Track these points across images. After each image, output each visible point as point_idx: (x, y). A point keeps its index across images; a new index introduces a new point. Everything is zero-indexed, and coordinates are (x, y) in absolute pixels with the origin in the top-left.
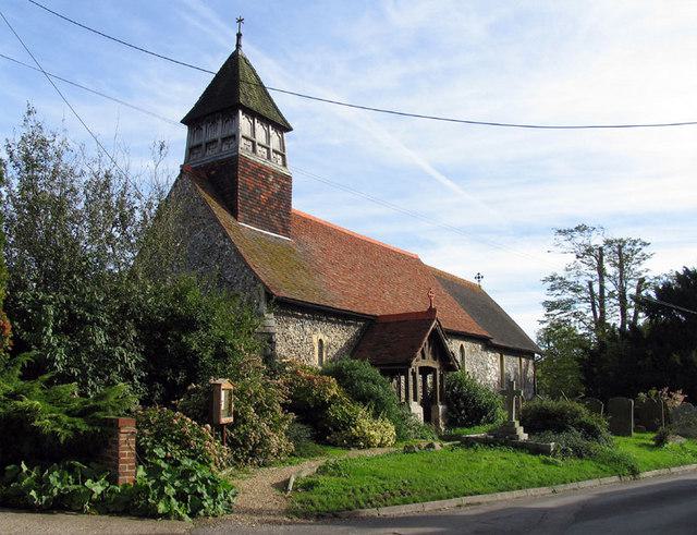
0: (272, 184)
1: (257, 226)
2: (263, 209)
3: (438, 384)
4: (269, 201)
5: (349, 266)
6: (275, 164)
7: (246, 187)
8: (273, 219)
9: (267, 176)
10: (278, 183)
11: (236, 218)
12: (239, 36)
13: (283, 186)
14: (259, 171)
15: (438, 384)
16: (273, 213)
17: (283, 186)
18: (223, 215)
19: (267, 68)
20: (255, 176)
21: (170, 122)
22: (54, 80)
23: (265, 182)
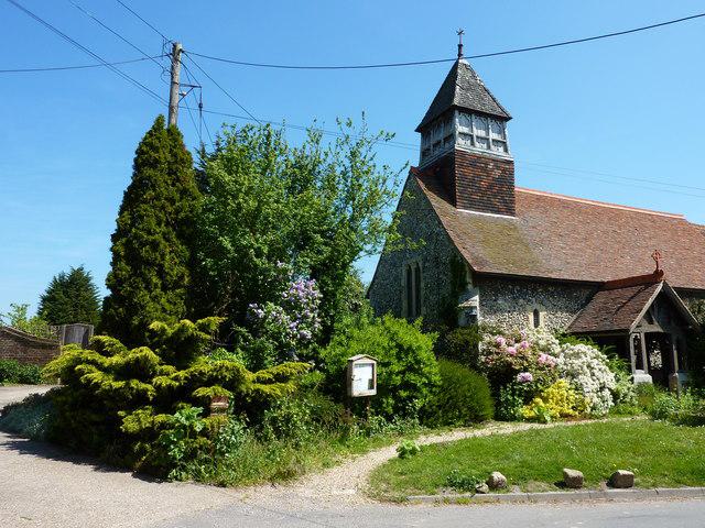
0: (492, 170)
1: (478, 209)
2: (484, 194)
3: (414, 284)
4: (490, 187)
5: (583, 235)
6: (498, 152)
7: (464, 177)
8: (495, 201)
9: (487, 164)
10: (498, 168)
11: (455, 206)
12: (460, 46)
13: (504, 171)
14: (477, 162)
15: (414, 284)
16: (495, 196)
17: (504, 171)
18: (437, 203)
19: (498, 80)
20: (474, 166)
21: (292, 126)
22: (192, 57)
23: (485, 170)
